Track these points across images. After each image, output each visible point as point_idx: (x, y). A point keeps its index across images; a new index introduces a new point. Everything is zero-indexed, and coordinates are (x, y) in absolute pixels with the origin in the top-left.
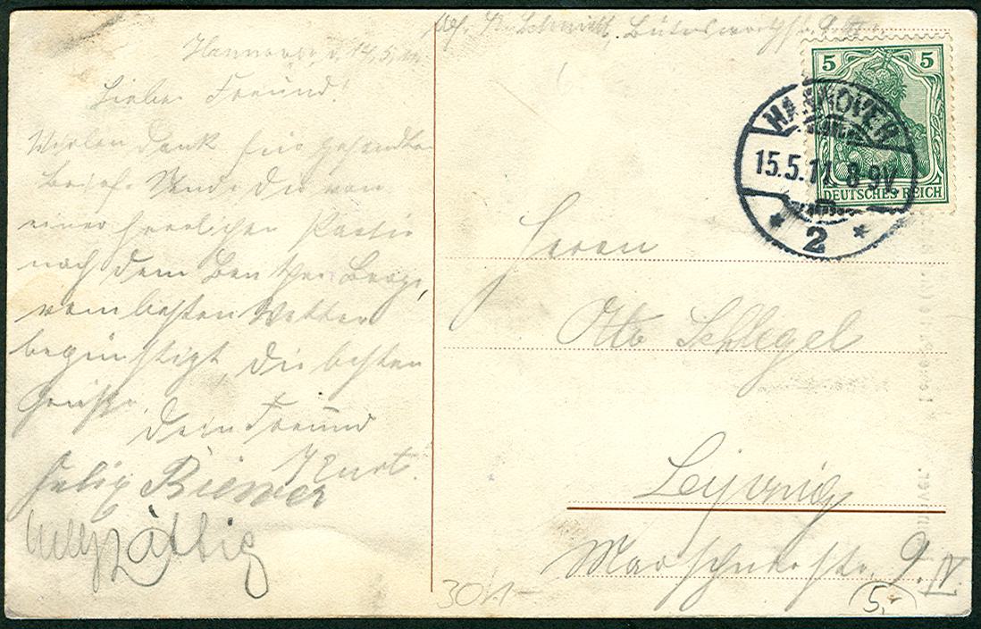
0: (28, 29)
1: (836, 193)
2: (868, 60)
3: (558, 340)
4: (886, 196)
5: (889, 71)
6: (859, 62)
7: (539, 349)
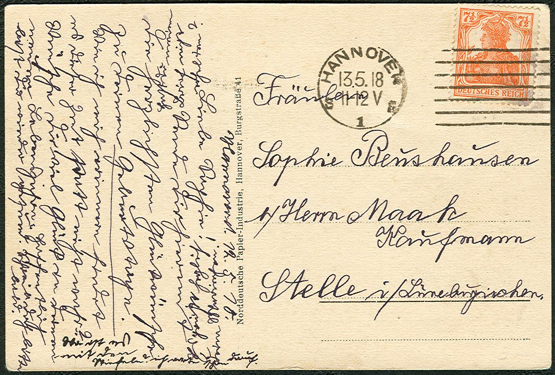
0: (546, 363)
1: (493, 91)
2: (490, 18)
3: (34, 105)
4: (493, 94)
5: (503, 25)
6: (486, 18)
7: (498, 339)
